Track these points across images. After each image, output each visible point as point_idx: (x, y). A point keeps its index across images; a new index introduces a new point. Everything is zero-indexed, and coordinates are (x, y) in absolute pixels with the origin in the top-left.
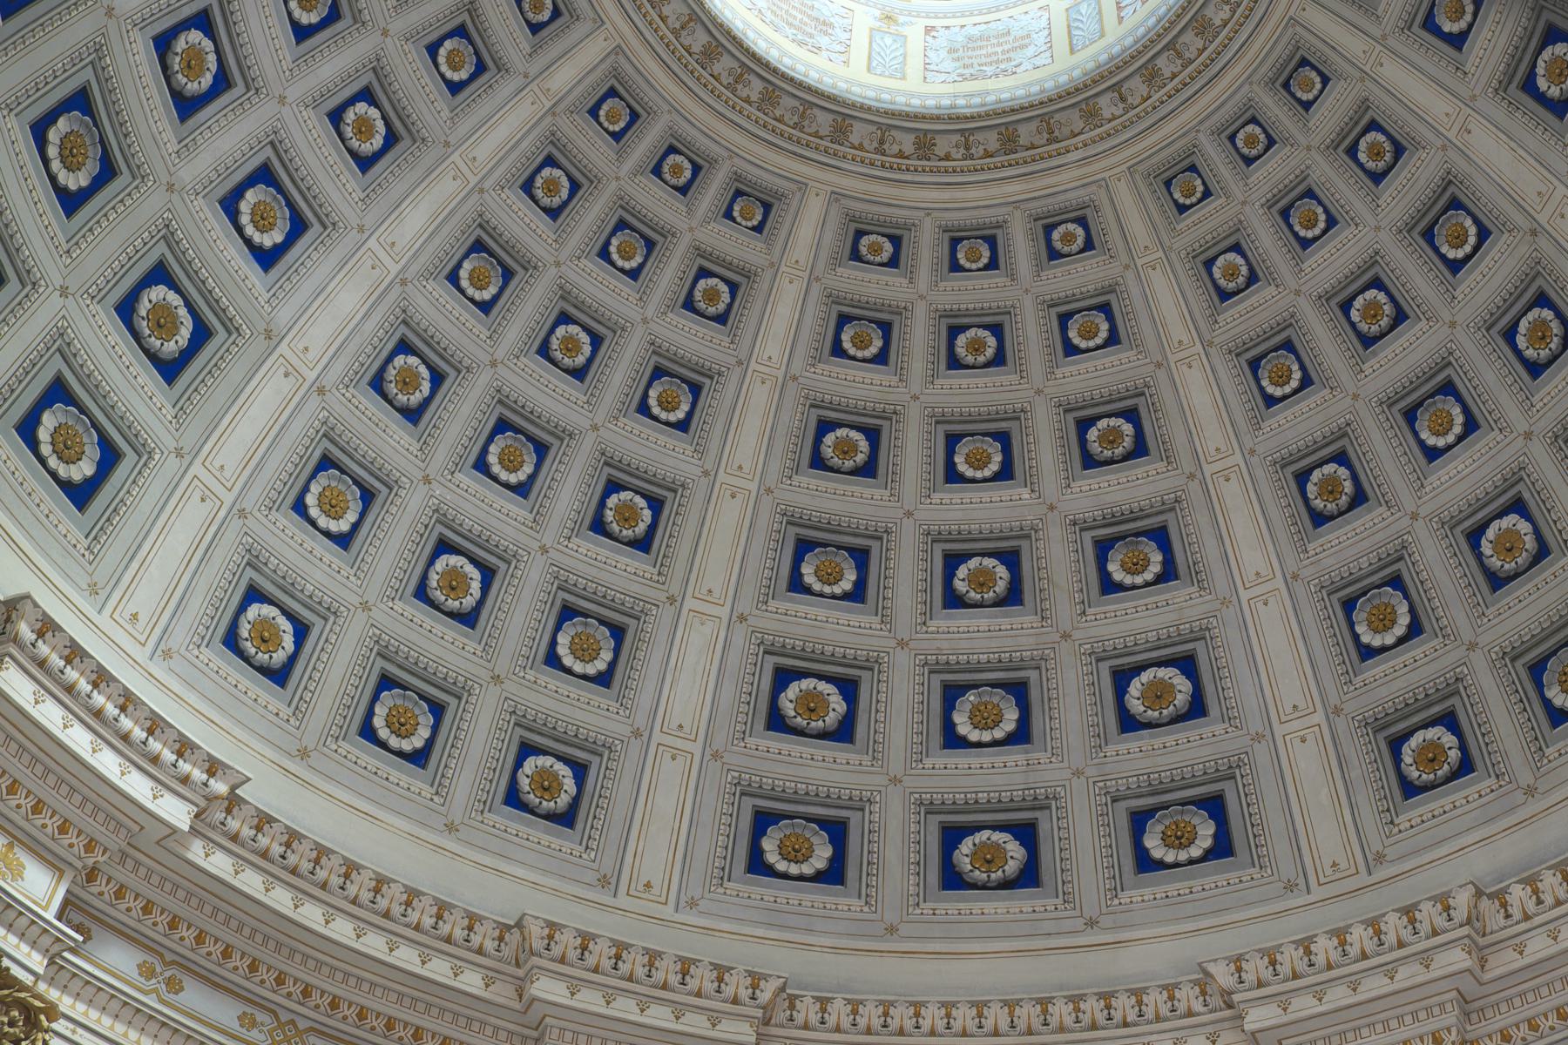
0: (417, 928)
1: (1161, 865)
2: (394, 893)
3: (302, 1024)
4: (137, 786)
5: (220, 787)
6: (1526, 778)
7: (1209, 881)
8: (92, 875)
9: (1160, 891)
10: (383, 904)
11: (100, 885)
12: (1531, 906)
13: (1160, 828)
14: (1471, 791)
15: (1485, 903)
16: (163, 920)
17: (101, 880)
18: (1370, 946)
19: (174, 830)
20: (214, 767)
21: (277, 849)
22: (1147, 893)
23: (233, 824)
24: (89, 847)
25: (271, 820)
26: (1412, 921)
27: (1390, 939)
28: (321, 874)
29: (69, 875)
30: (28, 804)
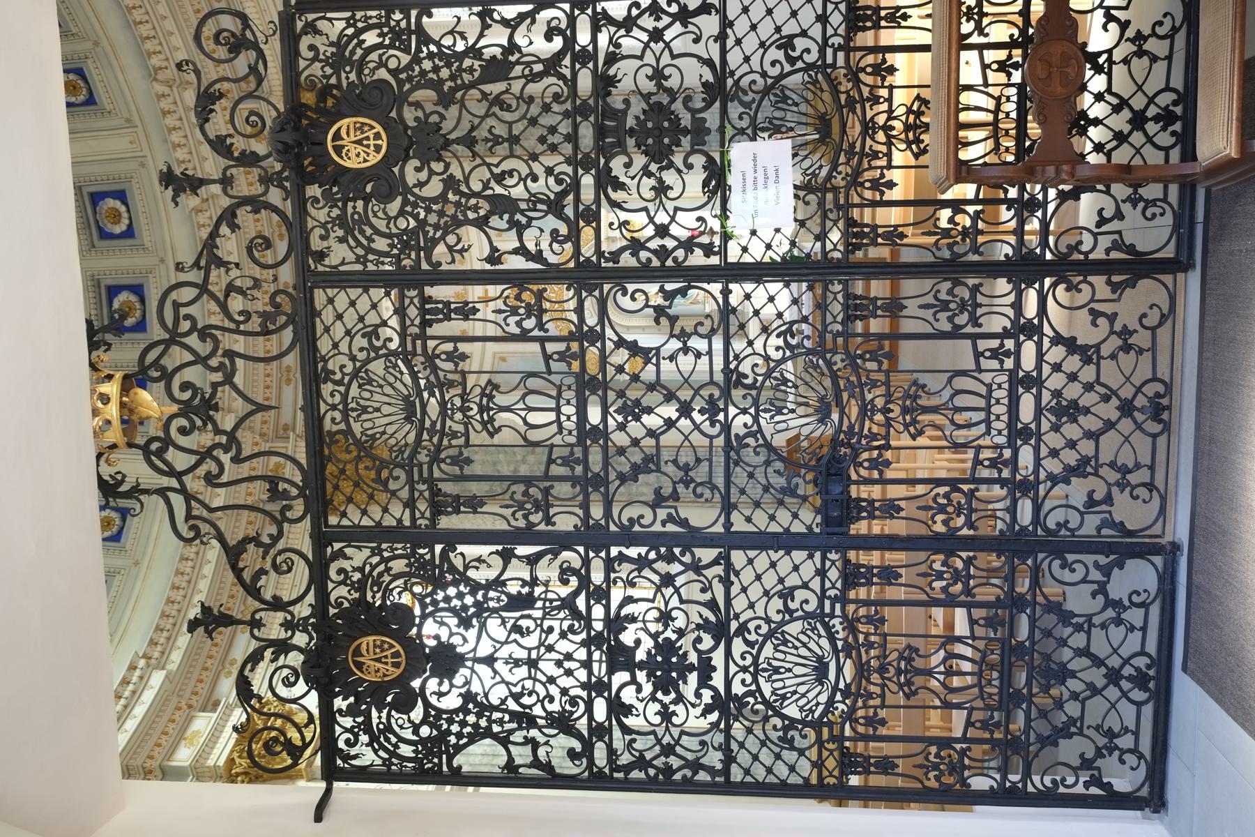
0: (193, 568)
1: (130, 226)
2: (178, 581)
3: (242, 608)
4: (148, 696)
5: (142, 663)
6: (88, 45)
7: (139, 204)
8: (190, 707)
9: (144, 228)
10: (184, 584)
11: (193, 702)
12: (162, 57)
13: (109, 225)
14: (94, 72)
15: (159, 77)
16: (204, 674)
17: (191, 702)
18: (181, 133)
19: (167, 676)
20: (133, 667)
21: (165, 634)
22: (145, 233)
23: (156, 655)
24: (179, 709)
25: (151, 640)
26: (169, 112)
27: (178, 124)
28: (174, 613)
29: (193, 713)
30: (164, 737)
